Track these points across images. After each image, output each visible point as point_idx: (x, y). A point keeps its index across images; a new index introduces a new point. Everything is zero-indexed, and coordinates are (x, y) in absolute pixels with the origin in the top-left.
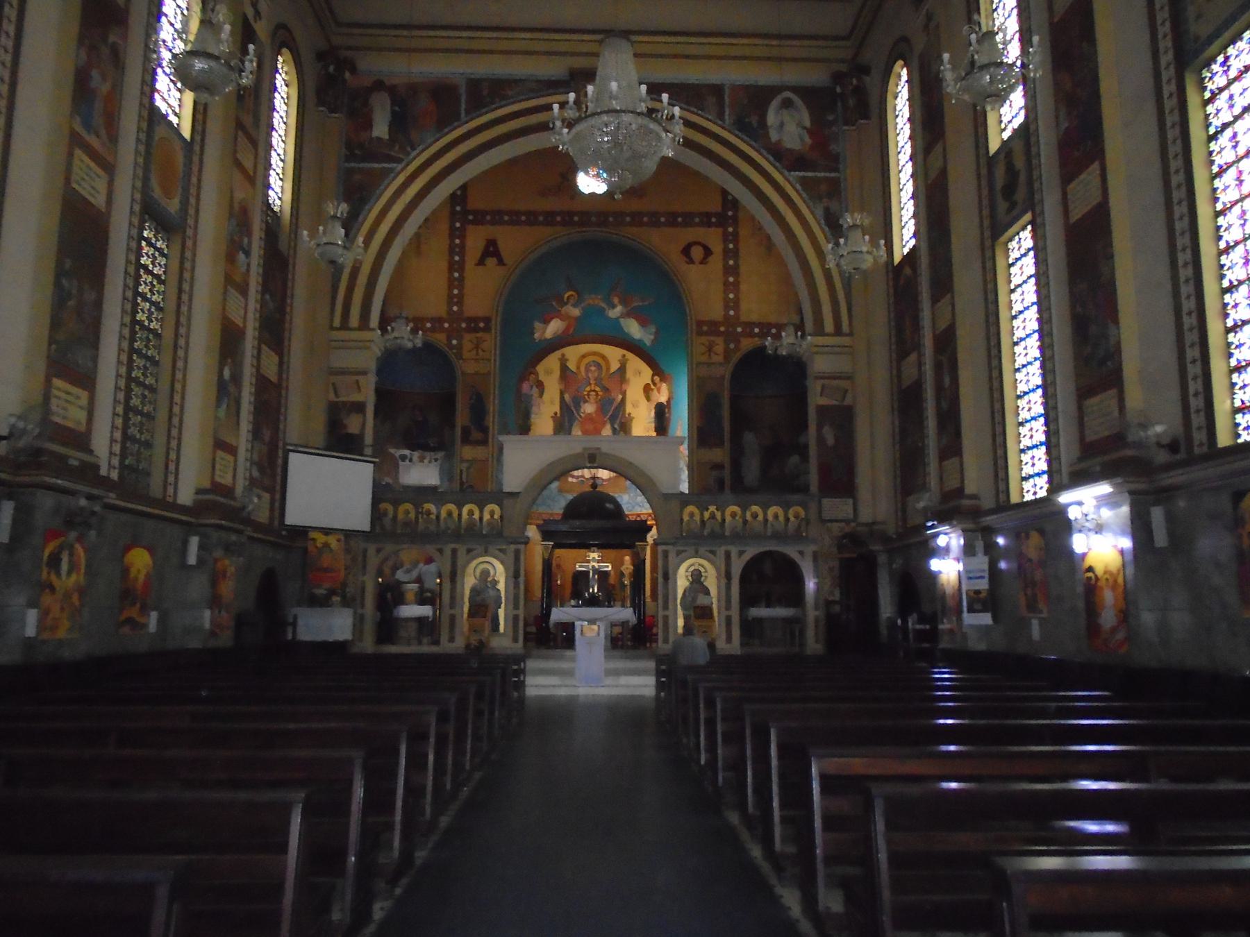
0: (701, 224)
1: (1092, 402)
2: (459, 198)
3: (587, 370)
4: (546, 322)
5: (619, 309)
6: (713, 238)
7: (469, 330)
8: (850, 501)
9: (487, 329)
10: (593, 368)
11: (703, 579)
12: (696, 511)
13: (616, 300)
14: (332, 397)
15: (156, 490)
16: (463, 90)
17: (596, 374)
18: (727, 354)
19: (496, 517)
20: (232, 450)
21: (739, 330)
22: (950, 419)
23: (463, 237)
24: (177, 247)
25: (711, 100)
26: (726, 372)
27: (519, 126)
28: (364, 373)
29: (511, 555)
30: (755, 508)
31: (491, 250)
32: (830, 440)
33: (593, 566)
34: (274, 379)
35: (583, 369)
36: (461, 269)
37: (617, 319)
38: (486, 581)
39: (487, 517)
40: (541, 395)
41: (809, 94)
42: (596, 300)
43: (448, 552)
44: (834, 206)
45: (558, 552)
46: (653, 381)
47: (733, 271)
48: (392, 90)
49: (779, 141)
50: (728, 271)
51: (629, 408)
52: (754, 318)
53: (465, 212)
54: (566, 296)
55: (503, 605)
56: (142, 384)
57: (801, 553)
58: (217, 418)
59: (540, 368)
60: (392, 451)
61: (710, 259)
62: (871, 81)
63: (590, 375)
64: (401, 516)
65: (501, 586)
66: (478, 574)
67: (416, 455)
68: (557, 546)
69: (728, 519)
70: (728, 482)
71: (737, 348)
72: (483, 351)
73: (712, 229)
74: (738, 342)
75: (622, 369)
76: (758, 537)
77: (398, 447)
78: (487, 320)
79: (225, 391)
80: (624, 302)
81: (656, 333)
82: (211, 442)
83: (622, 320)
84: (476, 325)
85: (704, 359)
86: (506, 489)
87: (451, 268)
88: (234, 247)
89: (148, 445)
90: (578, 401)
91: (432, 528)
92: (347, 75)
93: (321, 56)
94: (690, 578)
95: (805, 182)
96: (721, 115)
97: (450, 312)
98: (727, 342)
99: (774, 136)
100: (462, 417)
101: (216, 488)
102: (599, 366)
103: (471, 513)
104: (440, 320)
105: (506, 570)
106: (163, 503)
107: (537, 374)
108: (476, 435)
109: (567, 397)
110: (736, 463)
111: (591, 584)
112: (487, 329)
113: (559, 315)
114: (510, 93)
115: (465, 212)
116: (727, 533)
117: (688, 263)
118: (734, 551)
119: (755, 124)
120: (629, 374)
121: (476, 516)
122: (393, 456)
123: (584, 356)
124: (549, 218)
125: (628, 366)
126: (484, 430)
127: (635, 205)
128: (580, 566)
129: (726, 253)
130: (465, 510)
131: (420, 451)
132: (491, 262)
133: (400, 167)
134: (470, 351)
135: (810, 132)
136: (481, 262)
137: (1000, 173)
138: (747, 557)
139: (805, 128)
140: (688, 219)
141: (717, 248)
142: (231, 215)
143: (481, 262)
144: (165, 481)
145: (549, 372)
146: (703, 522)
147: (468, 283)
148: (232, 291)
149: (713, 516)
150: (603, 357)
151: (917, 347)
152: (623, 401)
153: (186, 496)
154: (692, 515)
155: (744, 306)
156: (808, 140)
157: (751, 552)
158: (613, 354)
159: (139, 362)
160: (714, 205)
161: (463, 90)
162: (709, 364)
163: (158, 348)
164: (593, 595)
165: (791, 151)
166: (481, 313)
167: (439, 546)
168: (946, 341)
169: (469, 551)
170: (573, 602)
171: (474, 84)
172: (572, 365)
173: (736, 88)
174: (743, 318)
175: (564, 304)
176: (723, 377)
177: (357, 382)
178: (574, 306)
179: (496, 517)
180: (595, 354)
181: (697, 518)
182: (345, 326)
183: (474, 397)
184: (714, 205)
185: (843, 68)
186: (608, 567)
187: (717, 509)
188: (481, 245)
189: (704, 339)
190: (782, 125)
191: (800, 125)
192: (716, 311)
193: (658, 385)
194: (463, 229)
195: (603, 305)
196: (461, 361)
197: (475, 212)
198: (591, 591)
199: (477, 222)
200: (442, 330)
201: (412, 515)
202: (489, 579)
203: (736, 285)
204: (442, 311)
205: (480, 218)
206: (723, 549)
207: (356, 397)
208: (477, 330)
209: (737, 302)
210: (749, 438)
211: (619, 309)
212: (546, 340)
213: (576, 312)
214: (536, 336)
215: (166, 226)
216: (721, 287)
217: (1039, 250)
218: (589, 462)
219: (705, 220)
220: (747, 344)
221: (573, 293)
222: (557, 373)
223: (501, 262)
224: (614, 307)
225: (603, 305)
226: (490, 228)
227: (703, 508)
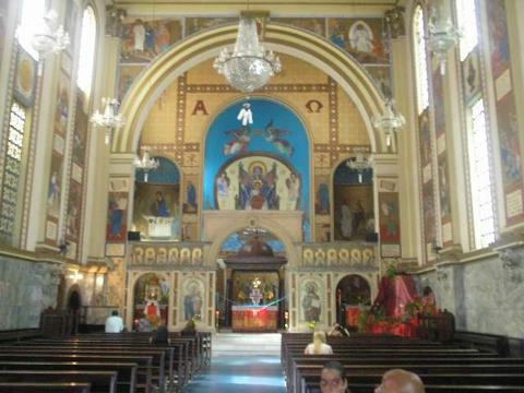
1: (509, 196)
2: (182, 79)
4: (231, 144)
6: (323, 98)
8: (398, 246)
9: (197, 150)
12: (311, 252)
14: (111, 190)
15: (15, 244)
16: (183, 24)
20: (55, 220)
22: (446, 201)
23: (184, 99)
24: (29, 118)
25: (318, 26)
26: (331, 172)
27: (200, 61)
28: (128, 176)
30: (344, 250)
31: (200, 106)
32: (386, 212)
34: (80, 181)
36: (184, 117)
39: (194, 255)
40: (228, 185)
41: (371, 22)
44: (386, 82)
47: (335, 116)
48: (146, 24)
50: (331, 116)
51: (278, 193)
52: (347, 142)
53: (186, 86)
56: (9, 188)
57: (370, 276)
58: (48, 204)
59: (228, 170)
62: (406, 15)
64: (147, 255)
67: (159, 219)
69: (329, 256)
70: (332, 236)
71: (337, 159)
73: (323, 93)
76: (347, 266)
78: (198, 145)
79: (53, 189)
82: (44, 217)
84: (190, 147)
85: (319, 165)
88: (60, 112)
89: (12, 219)
90: (249, 188)
91: (164, 261)
92: (122, 17)
93: (109, 8)
95: (369, 69)
96: (324, 35)
98: (331, 155)
99: (353, 45)
100: (183, 198)
101: (48, 241)
103: (185, 253)
105: (205, 284)
106: (18, 250)
107: (225, 173)
108: (191, 209)
109: (243, 186)
110: (338, 226)
113: (237, 140)
118: (332, 274)
119: (342, 38)
126: (196, 206)
127: (280, 81)
130: (182, 251)
132: (200, 112)
133: (148, 65)
135: (373, 42)
136: (194, 113)
137: (466, 69)
138: (137, 276)
140: (309, 88)
141: (325, 103)
142: (58, 96)
143: (194, 113)
144: (22, 226)
146: (315, 258)
148: (58, 136)
149: (320, 255)
151: (430, 161)
152: (274, 189)
153: (31, 247)
155: (340, 135)
156: (372, 47)
157: (341, 275)
158: (269, 162)
159: (8, 176)
160: (325, 81)
161: (183, 24)
163: (18, 168)
165: (361, 52)
166: (193, 141)
168: (444, 160)
171: (189, 20)
172: (245, 168)
173: (331, 19)
176: (329, 175)
178: (247, 135)
181: (312, 256)
182: (118, 152)
184: (325, 81)
185: (390, 8)
188: (195, 103)
189: (319, 154)
190: (357, 39)
191: (367, 39)
192: (324, 138)
194: (185, 95)
199: (192, 91)
200: (172, 150)
201: (154, 254)
204: (173, 141)
205: (194, 88)
206: (326, 273)
207: (123, 190)
208: (193, 150)
210: (345, 208)
215: (23, 105)
216: (328, 125)
217: (487, 112)
220: (343, 157)
222: (237, 173)
223: (205, 113)
224: (268, 136)
226: (200, 94)
227: (315, 250)
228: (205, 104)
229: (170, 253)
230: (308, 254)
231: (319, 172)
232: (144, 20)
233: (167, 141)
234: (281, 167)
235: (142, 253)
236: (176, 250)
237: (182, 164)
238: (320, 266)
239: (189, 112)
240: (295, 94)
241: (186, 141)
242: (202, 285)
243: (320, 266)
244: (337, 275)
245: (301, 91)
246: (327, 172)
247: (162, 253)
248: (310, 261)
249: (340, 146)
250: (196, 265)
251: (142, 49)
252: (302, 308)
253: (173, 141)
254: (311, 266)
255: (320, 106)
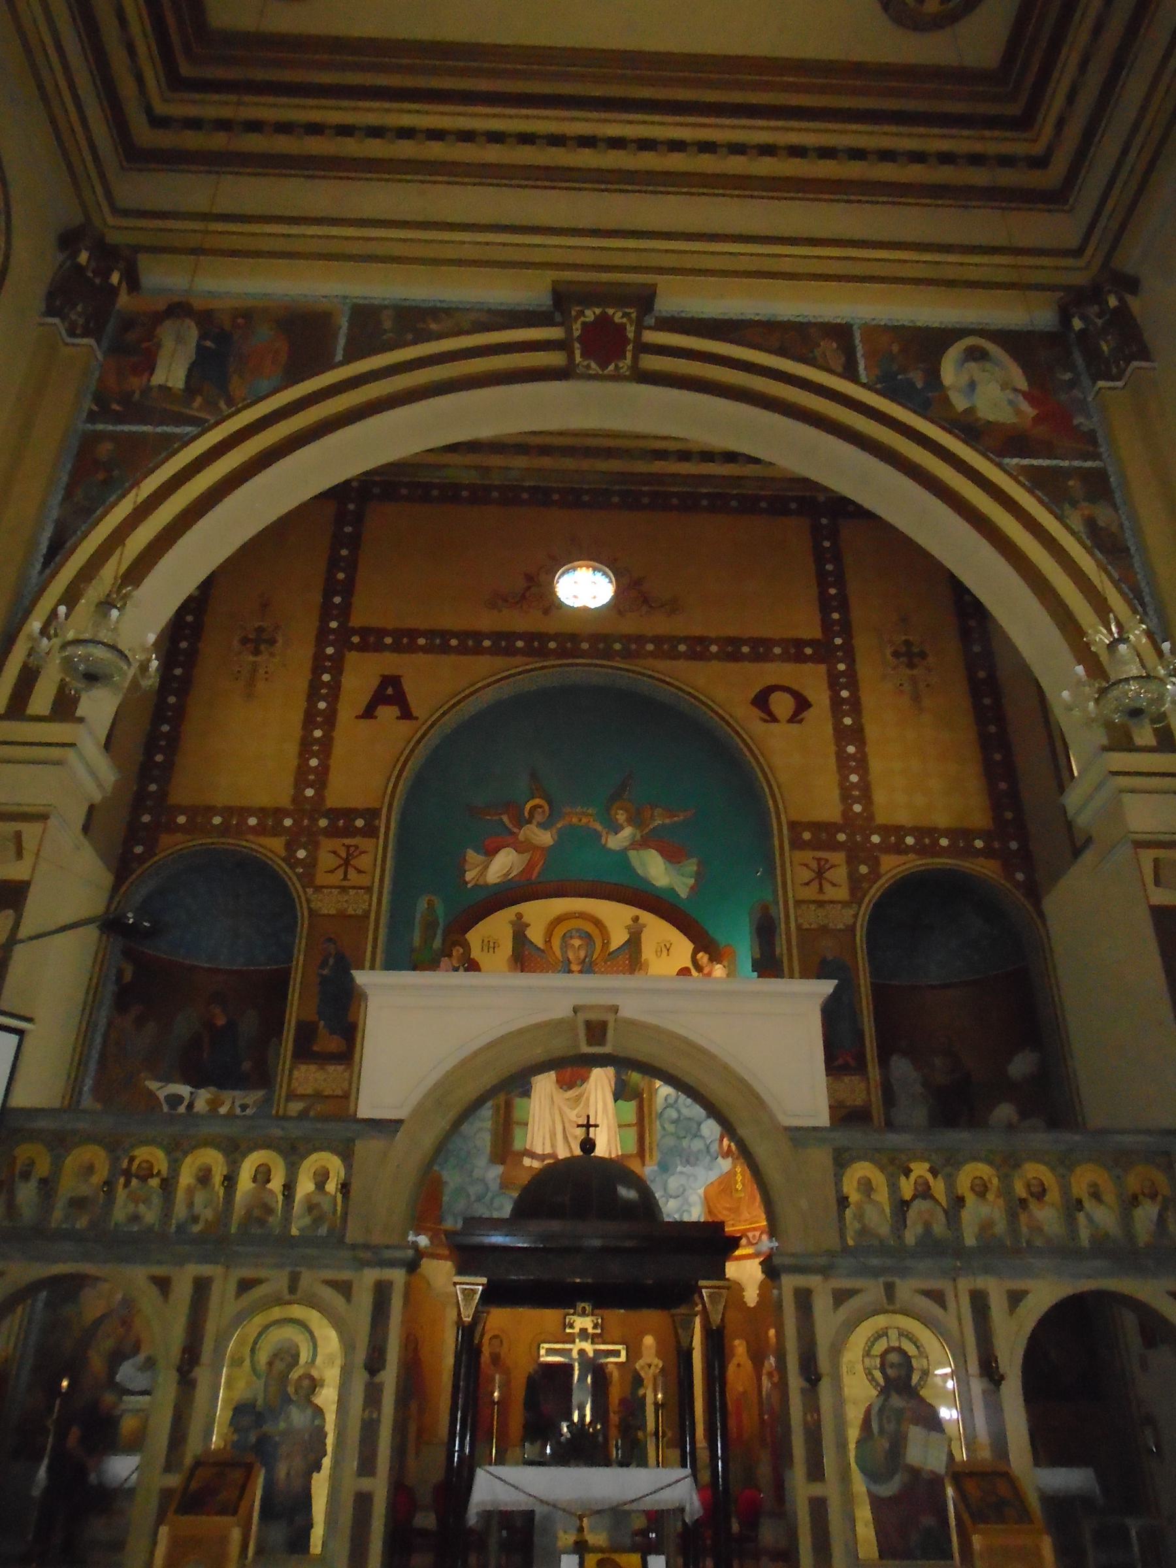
0: (786, 658)
3: (565, 945)
4: (491, 852)
5: (627, 832)
7: (333, 832)
9: (370, 831)
10: (577, 942)
11: (915, 1379)
12: (879, 1179)
13: (621, 817)
17: (582, 954)
18: (856, 885)
19: (331, 1187)
21: (876, 839)
23: (337, 669)
25: (829, 348)
29: (364, 1299)
33: (582, 1352)
35: (556, 943)
36: (330, 720)
37: (623, 852)
38: (284, 1378)
39: (305, 1186)
42: (584, 817)
43: (183, 1290)
44: (1104, 515)
45: (499, 1318)
46: (695, 961)
48: (205, 319)
49: (970, 411)
50: (842, 735)
52: (903, 818)
54: (528, 806)
55: (327, 1462)
59: (474, 936)
60: (153, 1085)
61: (808, 715)
63: (571, 956)
64: (69, 1186)
65: (327, 1397)
66: (263, 1357)
68: (495, 1296)
71: (875, 874)
72: (360, 872)
73: (809, 667)
74: (875, 864)
75: (634, 942)
77: (168, 1079)
78: (371, 814)
80: (636, 819)
81: (699, 876)
83: (632, 854)
85: (810, 893)
86: (365, 1111)
87: (310, 720)
91: (150, 1216)
94: (878, 1374)
97: (298, 798)
102: (588, 938)
103: (263, 1175)
104: (279, 813)
105: (348, 1346)
107: (466, 946)
108: (329, 1042)
111: (575, 1401)
112: (370, 831)
114: (433, 326)
115: (345, 632)
116: (970, 1240)
117: (765, 721)
118: (996, 1290)
120: (648, 951)
121: (276, 1184)
122: (152, 1095)
123: (559, 920)
124: (503, 643)
125: (644, 937)
128: (550, 1352)
129: (836, 703)
131: (212, 1089)
132: (387, 713)
134: (332, 871)
136: (369, 713)
139: (1015, 390)
140: (761, 649)
141: (820, 697)
143: (369, 713)
145: (491, 946)
146: (901, 1207)
147: (340, 749)
149: (924, 1192)
150: (598, 923)
154: (867, 1187)
156: (1029, 411)
162: (820, 904)
164: (579, 1430)
167: (159, 1271)
169: (245, 1286)
170: (530, 1450)
172: (536, 935)
173: (873, 331)
174: (881, 819)
175: (521, 821)
176: (852, 929)
177: (18, 836)
178: (544, 826)
179: (331, 1187)
180: (582, 916)
181: (882, 1195)
183: (331, 961)
186: (617, 1353)
187: (934, 1172)
189: (808, 856)
190: (972, 386)
192: (828, 808)
193: (706, 971)
195: (599, 827)
196: (310, 891)
197: (364, 632)
198: (576, 1418)
199: (363, 648)
200: (277, 831)
202: (295, 1375)
203: (862, 763)
204: (282, 796)
205: (372, 640)
206: (965, 1284)
208: (349, 831)
209: (865, 788)
211: (627, 832)
212: (486, 886)
213: (546, 838)
214: (469, 876)
218: (590, 1043)
219: (793, 651)
221: (546, 807)
223: (406, 714)
224: (616, 829)
225: (599, 827)
227: (897, 1167)
228: (408, 686)
229: (186, 1178)
230: (867, 1187)
231: (812, 918)
232: (198, 304)
233: (264, 799)
234: (658, 930)
235: (43, 1168)
236: (214, 1159)
237: (308, 879)
238: (931, 1247)
239: (346, 713)
240: (716, 665)
241: (333, 800)
242: (330, 1340)
243: (931, 1247)
244: (1015, 1299)
245: (735, 657)
246: (841, 918)
247: (146, 1174)
248: (879, 1220)
249: (885, 830)
250: (306, 1240)
251: (180, 384)
252: (859, 1485)
253: (282, 796)
254: (883, 1249)
255: (802, 704)
